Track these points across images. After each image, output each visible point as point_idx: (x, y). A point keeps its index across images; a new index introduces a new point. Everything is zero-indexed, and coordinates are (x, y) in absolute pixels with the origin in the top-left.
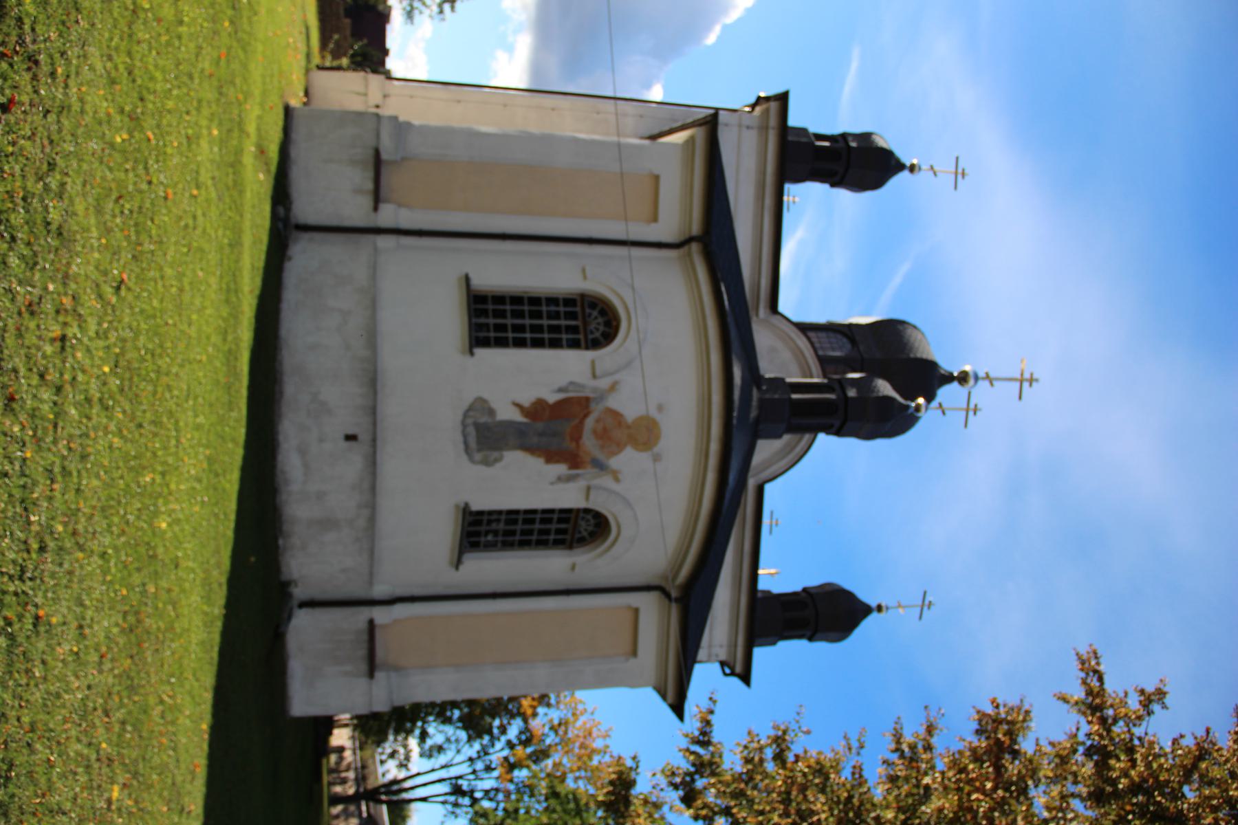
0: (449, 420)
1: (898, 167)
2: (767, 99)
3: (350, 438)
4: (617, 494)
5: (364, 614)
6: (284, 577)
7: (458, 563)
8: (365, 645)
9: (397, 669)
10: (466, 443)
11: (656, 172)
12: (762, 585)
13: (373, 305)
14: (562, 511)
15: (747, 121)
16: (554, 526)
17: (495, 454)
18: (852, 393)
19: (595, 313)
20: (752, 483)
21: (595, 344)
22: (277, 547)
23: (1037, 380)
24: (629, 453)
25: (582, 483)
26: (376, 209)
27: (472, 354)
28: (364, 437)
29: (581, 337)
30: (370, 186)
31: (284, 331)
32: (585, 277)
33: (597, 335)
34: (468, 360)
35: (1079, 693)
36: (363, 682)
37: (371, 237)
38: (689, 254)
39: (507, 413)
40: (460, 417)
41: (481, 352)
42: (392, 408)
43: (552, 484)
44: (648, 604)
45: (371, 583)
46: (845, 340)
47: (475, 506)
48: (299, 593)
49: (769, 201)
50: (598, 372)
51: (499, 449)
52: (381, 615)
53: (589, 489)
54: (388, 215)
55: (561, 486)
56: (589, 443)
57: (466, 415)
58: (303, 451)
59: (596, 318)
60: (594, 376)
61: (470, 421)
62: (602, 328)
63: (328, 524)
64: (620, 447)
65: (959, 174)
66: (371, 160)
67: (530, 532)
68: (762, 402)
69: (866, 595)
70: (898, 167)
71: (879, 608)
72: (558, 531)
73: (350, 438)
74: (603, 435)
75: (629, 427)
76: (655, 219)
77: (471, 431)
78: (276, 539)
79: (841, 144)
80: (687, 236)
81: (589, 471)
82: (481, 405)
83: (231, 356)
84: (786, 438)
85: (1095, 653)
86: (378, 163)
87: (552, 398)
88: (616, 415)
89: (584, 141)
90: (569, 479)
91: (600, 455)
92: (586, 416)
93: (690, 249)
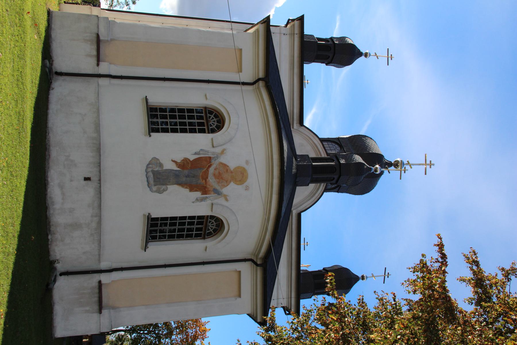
0: (140, 170)
1: (360, 54)
2: (293, 20)
3: (87, 179)
4: (227, 207)
5: (96, 277)
6: (52, 258)
7: (145, 248)
8: (97, 295)
9: (114, 308)
10: (148, 181)
11: (240, 48)
12: (304, 266)
13: (98, 111)
14: (199, 217)
15: (284, 31)
16: (195, 227)
17: (164, 187)
18: (342, 161)
19: (212, 116)
20: (294, 212)
21: (213, 131)
22: (48, 240)
23: (433, 165)
24: (232, 186)
25: (209, 202)
26: (98, 65)
27: (150, 136)
28: (94, 178)
29: (206, 127)
30: (95, 53)
31: (50, 124)
32: (206, 98)
33: (214, 127)
34: (148, 138)
35: (469, 275)
36: (96, 316)
37: (96, 79)
38: (258, 88)
39: (169, 166)
40: (145, 168)
41: (152, 134)
42: (107, 163)
43: (193, 202)
44: (246, 268)
45: (99, 261)
46: (336, 146)
47: (153, 216)
48: (60, 267)
49: (296, 70)
50: (215, 145)
51: (166, 184)
52: (105, 278)
53: (212, 204)
54: (104, 68)
55: (198, 203)
56: (212, 181)
57: (147, 167)
58: (61, 187)
59: (213, 118)
60: (213, 147)
61: (150, 170)
62: (216, 123)
63: (76, 226)
64: (228, 183)
65: (389, 57)
66: (95, 40)
67: (183, 230)
68: (297, 166)
69: (356, 271)
70: (360, 54)
71: (363, 278)
72: (198, 229)
73: (87, 179)
74: (219, 176)
75: (232, 172)
76: (240, 70)
77: (151, 174)
78: (47, 235)
79: (331, 43)
80: (257, 79)
81: (212, 195)
82: (155, 162)
83: (20, 115)
84: (312, 186)
85: (474, 252)
86: (98, 41)
87: (192, 158)
88: (225, 165)
89: (204, 31)
90: (202, 200)
91: (218, 187)
92: (210, 166)
93: (258, 85)
